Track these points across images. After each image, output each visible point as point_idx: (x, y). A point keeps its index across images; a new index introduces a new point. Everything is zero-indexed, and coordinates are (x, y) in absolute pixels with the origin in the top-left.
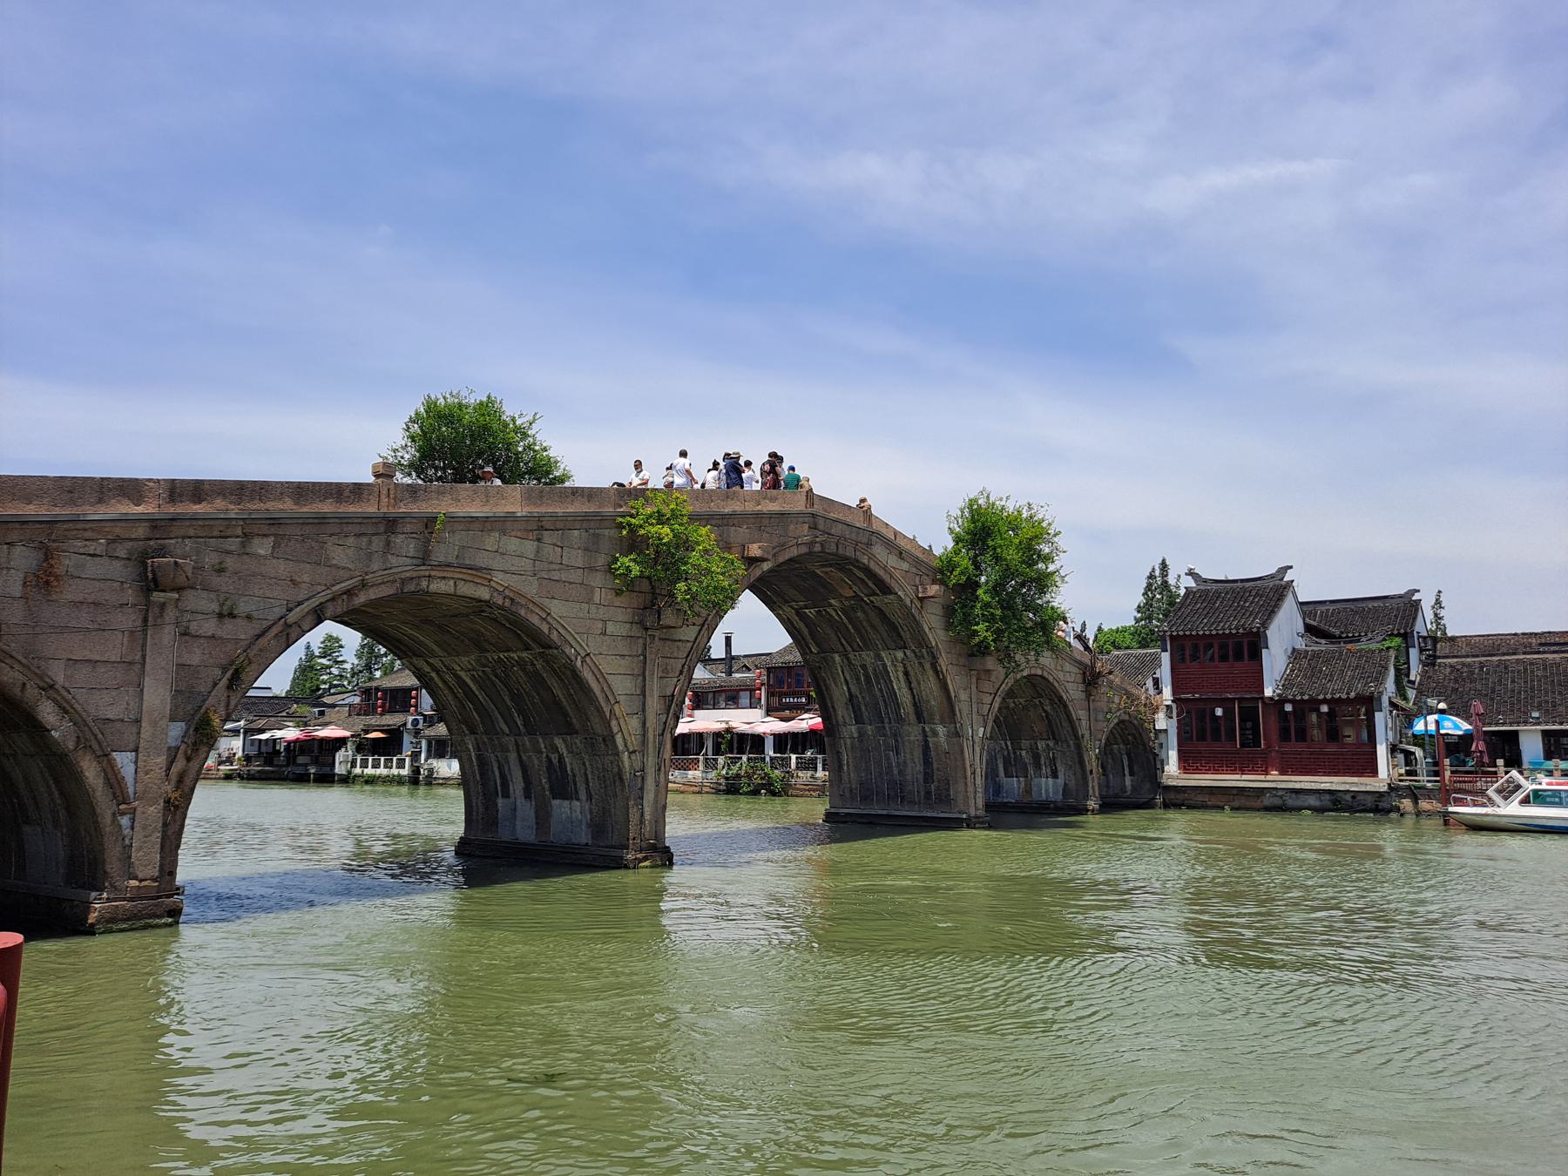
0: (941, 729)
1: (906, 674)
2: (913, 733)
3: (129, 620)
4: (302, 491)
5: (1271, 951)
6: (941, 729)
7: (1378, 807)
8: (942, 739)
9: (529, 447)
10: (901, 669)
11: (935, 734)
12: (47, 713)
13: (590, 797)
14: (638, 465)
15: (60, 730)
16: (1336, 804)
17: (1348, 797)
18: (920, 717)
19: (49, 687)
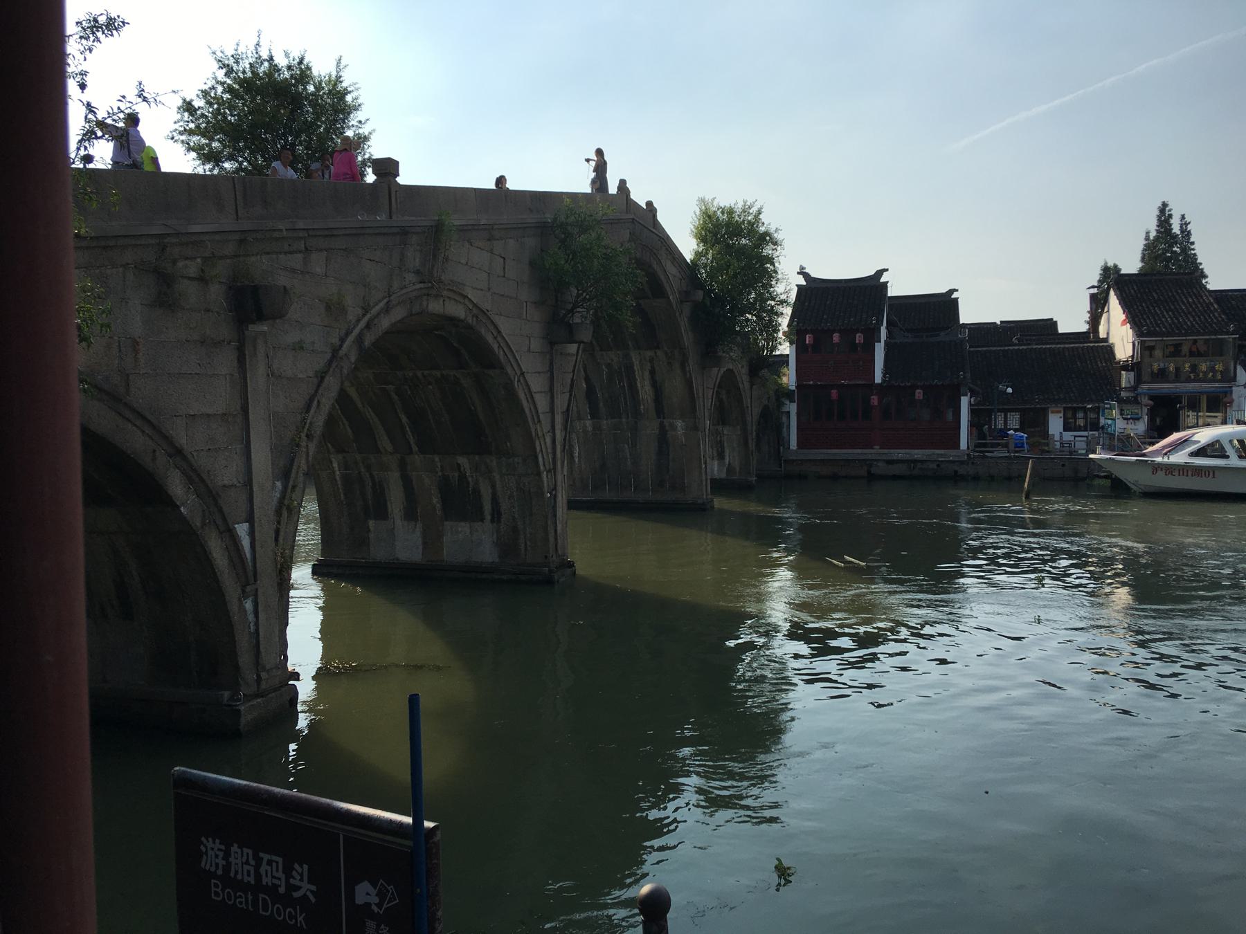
0: (679, 424)
1: (653, 372)
2: (650, 429)
3: (225, 362)
4: (846, 281)
5: (1154, 610)
6: (679, 424)
7: (954, 477)
8: (680, 432)
9: (318, 87)
10: (648, 366)
11: (674, 428)
12: (176, 486)
13: (496, 515)
14: (588, 160)
15: (188, 504)
16: (918, 476)
17: (934, 466)
18: (660, 411)
19: (177, 452)
